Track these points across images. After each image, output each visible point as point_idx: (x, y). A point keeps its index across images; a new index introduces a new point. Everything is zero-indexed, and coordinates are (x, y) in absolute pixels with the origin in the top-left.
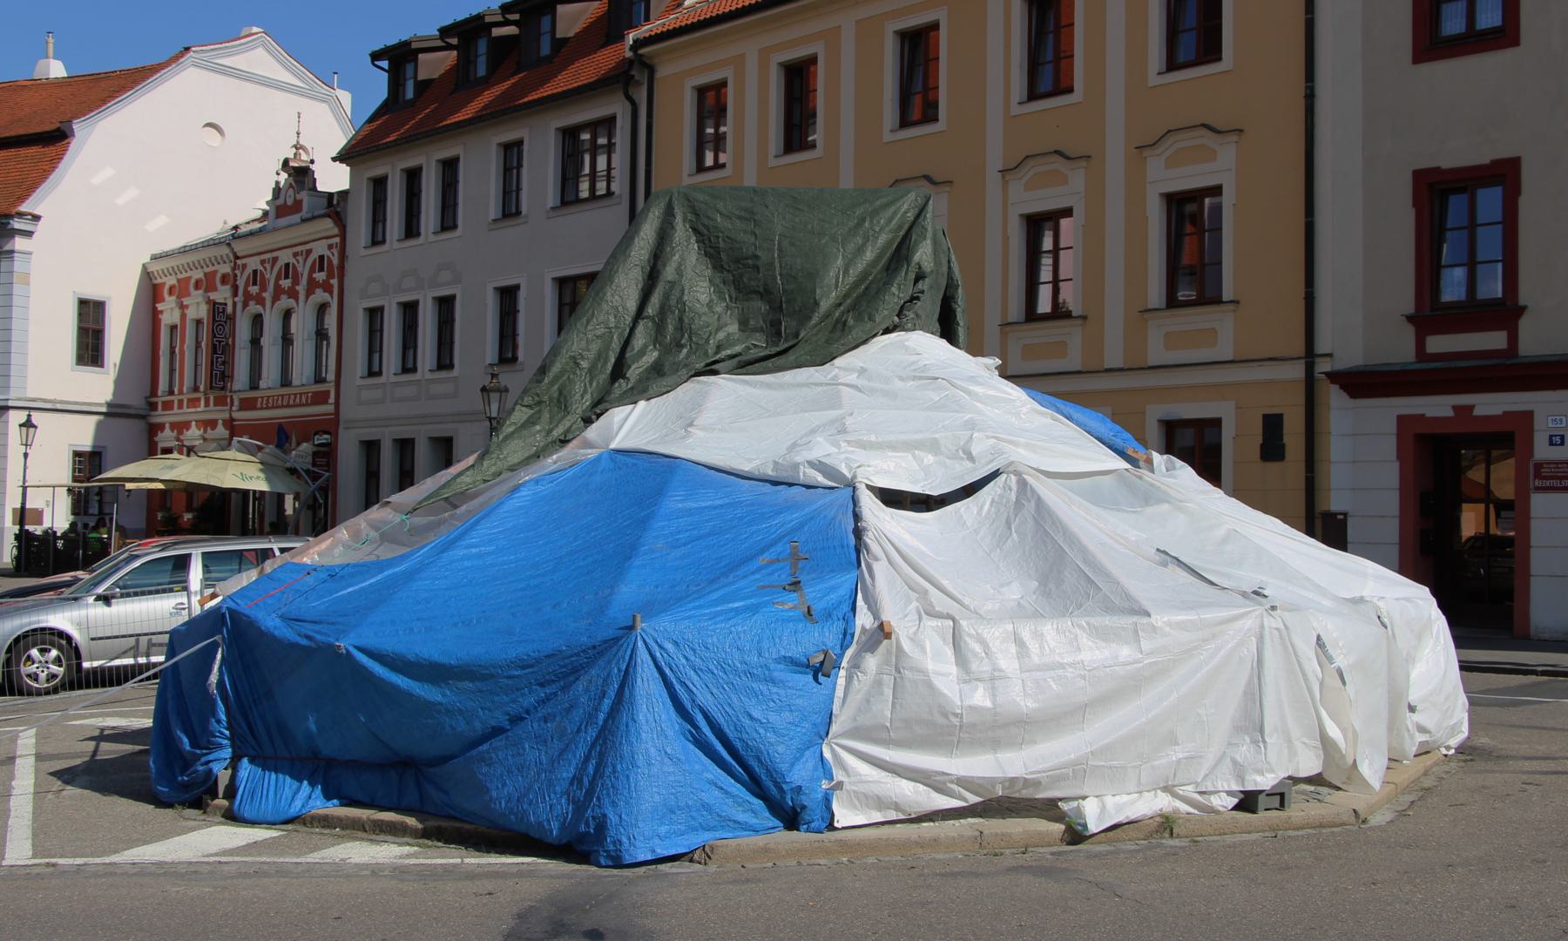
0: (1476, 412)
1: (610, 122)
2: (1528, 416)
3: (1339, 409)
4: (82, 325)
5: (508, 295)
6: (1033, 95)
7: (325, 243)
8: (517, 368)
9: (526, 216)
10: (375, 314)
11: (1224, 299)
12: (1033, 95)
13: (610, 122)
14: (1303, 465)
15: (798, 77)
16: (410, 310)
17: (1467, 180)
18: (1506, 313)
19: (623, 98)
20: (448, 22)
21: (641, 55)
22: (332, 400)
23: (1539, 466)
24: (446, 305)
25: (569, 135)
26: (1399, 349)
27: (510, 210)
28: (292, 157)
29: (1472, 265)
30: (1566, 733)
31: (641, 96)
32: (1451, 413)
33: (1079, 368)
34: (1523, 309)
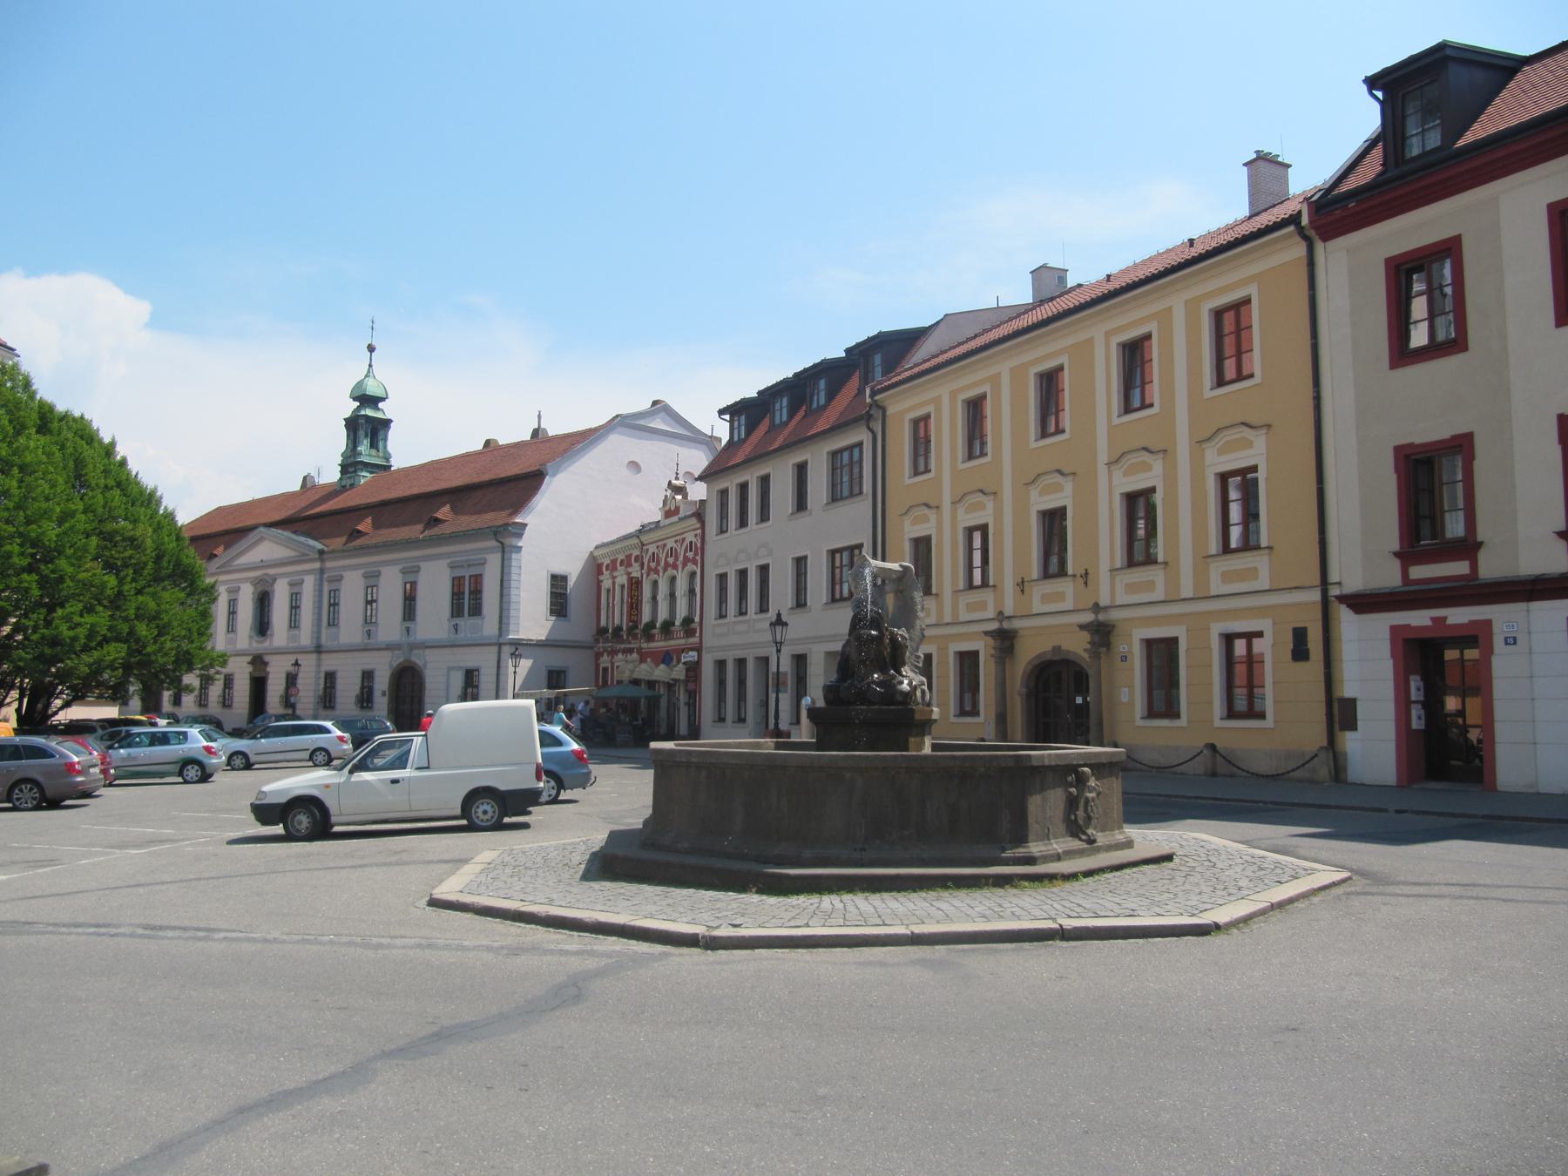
0: (1450, 621)
1: (860, 445)
5: (800, 562)
7: (692, 533)
10: (723, 578)
11: (1262, 546)
13: (860, 445)
14: (1322, 664)
15: (1050, 382)
18: (1468, 547)
20: (722, 406)
21: (876, 401)
22: (698, 634)
24: (764, 570)
26: (1389, 576)
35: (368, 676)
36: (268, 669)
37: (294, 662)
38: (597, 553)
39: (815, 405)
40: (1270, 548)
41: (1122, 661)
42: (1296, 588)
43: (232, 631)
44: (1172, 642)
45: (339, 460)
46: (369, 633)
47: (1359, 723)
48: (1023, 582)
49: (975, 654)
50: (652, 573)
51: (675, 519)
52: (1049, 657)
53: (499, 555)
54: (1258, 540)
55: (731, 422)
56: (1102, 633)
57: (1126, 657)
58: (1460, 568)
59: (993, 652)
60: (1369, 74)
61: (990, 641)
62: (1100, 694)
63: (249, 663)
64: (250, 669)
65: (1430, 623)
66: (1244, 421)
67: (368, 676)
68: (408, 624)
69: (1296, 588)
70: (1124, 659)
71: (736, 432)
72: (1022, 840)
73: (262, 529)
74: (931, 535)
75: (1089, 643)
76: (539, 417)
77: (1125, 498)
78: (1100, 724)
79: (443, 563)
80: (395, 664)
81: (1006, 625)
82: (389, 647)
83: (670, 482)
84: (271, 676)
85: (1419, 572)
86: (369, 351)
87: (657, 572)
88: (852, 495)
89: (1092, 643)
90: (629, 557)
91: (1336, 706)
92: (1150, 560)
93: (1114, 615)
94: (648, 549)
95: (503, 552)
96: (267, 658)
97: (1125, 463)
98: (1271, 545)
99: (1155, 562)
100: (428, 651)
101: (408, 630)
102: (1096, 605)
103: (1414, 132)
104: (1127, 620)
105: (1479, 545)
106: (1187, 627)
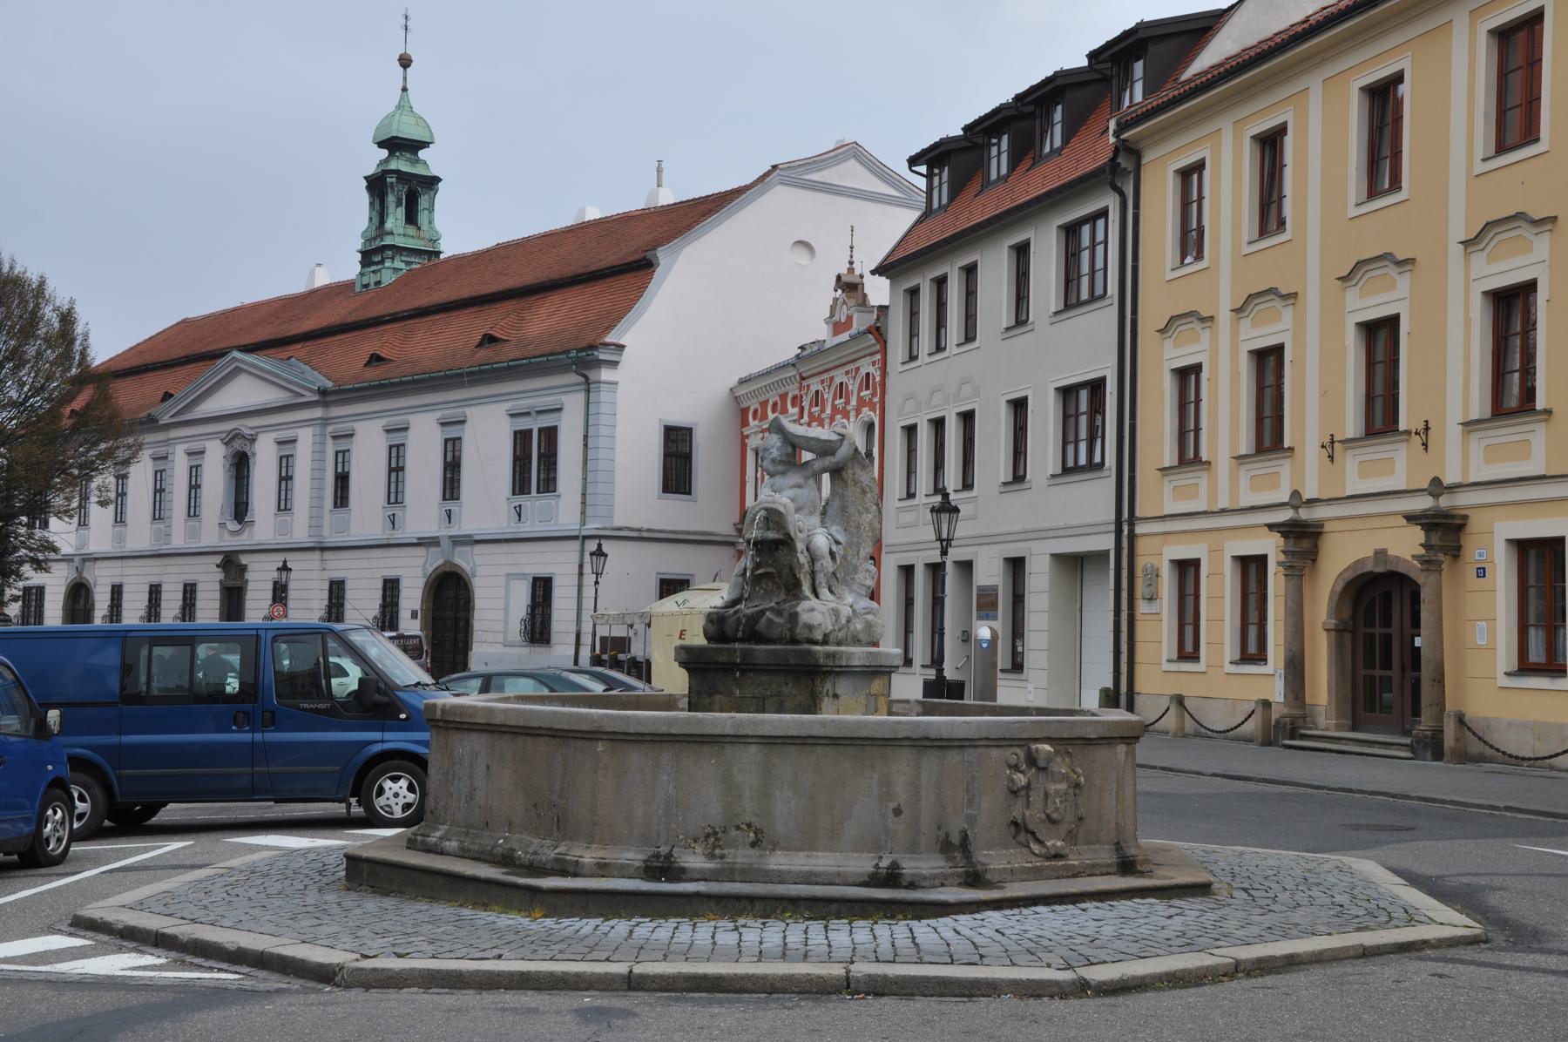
1: (1104, 213)
4: (673, 449)
5: (1019, 406)
6: (1501, 148)
7: (869, 360)
8: (1026, 486)
10: (911, 431)
12: (1501, 148)
13: (1104, 213)
16: (938, 424)
21: (1124, 141)
24: (967, 418)
25: (1071, 231)
27: (1021, 319)
28: (846, 272)
30: (1565, 958)
35: (391, 587)
36: (248, 576)
37: (280, 565)
38: (740, 392)
39: (1047, 149)
41: (1478, 576)
43: (195, 515)
45: (359, 243)
46: (393, 520)
49: (1261, 560)
50: (838, 417)
51: (845, 337)
52: (1369, 567)
53: (581, 396)
55: (929, 176)
57: (1484, 569)
62: (1440, 632)
63: (218, 566)
64: (219, 575)
67: (391, 587)
68: (450, 505)
70: (1481, 573)
71: (936, 193)
73: (236, 354)
75: (1421, 545)
76: (659, 170)
78: (1439, 680)
79: (501, 409)
80: (431, 570)
82: (422, 543)
83: (839, 278)
84: (250, 586)
86: (401, 65)
87: (846, 415)
88: (1093, 298)
90: (783, 397)
93: (1464, 500)
94: (808, 386)
95: (588, 391)
96: (244, 559)
98: (1548, 407)
100: (479, 549)
101: (449, 514)
102: (1436, 482)
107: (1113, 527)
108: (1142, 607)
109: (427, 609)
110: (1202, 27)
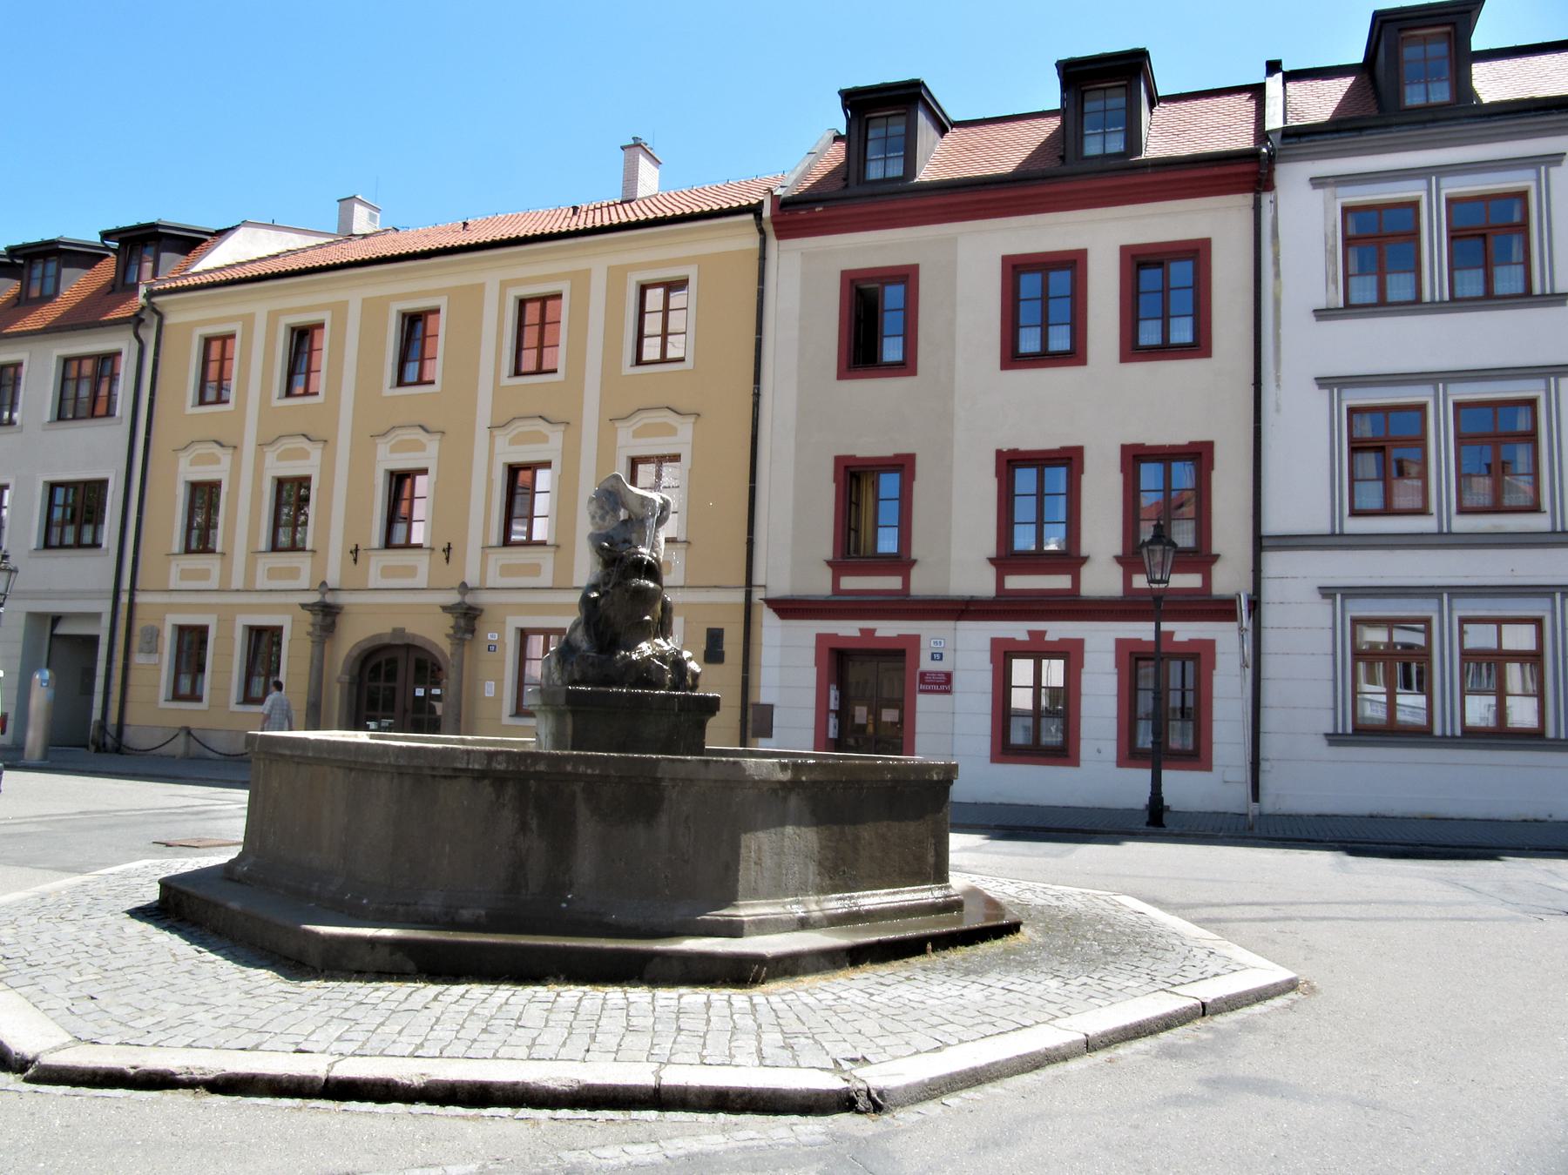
0: (878, 634)
2: (915, 640)
3: (770, 627)
9: (22, 426)
11: (307, 548)
13: (113, 356)
14: (740, 668)
15: (302, 338)
17: (1040, 461)
18: (901, 563)
19: (133, 337)
20: (111, 227)
21: (154, 303)
23: (923, 674)
26: (819, 584)
29: (1040, 523)
31: (150, 337)
32: (858, 634)
33: (550, 585)
34: (914, 562)
40: (313, 551)
42: (715, 587)
44: (202, 631)
47: (775, 731)
48: (357, 550)
52: (386, 641)
54: (215, 545)
56: (467, 618)
58: (893, 583)
59: (310, 629)
60: (843, 88)
61: (307, 616)
65: (858, 634)
66: (422, 423)
69: (715, 587)
72: (730, 899)
74: (220, 482)
75: (452, 627)
77: (506, 469)
81: (329, 599)
85: (849, 583)
89: (456, 628)
91: (750, 712)
92: (295, 547)
93: (483, 599)
97: (393, 439)
99: (213, 551)
103: (875, 157)
104: (501, 604)
105: (913, 562)
106: (219, 616)
107: (111, 595)
108: (138, 659)
109: (437, 1085)
110: (190, 242)
